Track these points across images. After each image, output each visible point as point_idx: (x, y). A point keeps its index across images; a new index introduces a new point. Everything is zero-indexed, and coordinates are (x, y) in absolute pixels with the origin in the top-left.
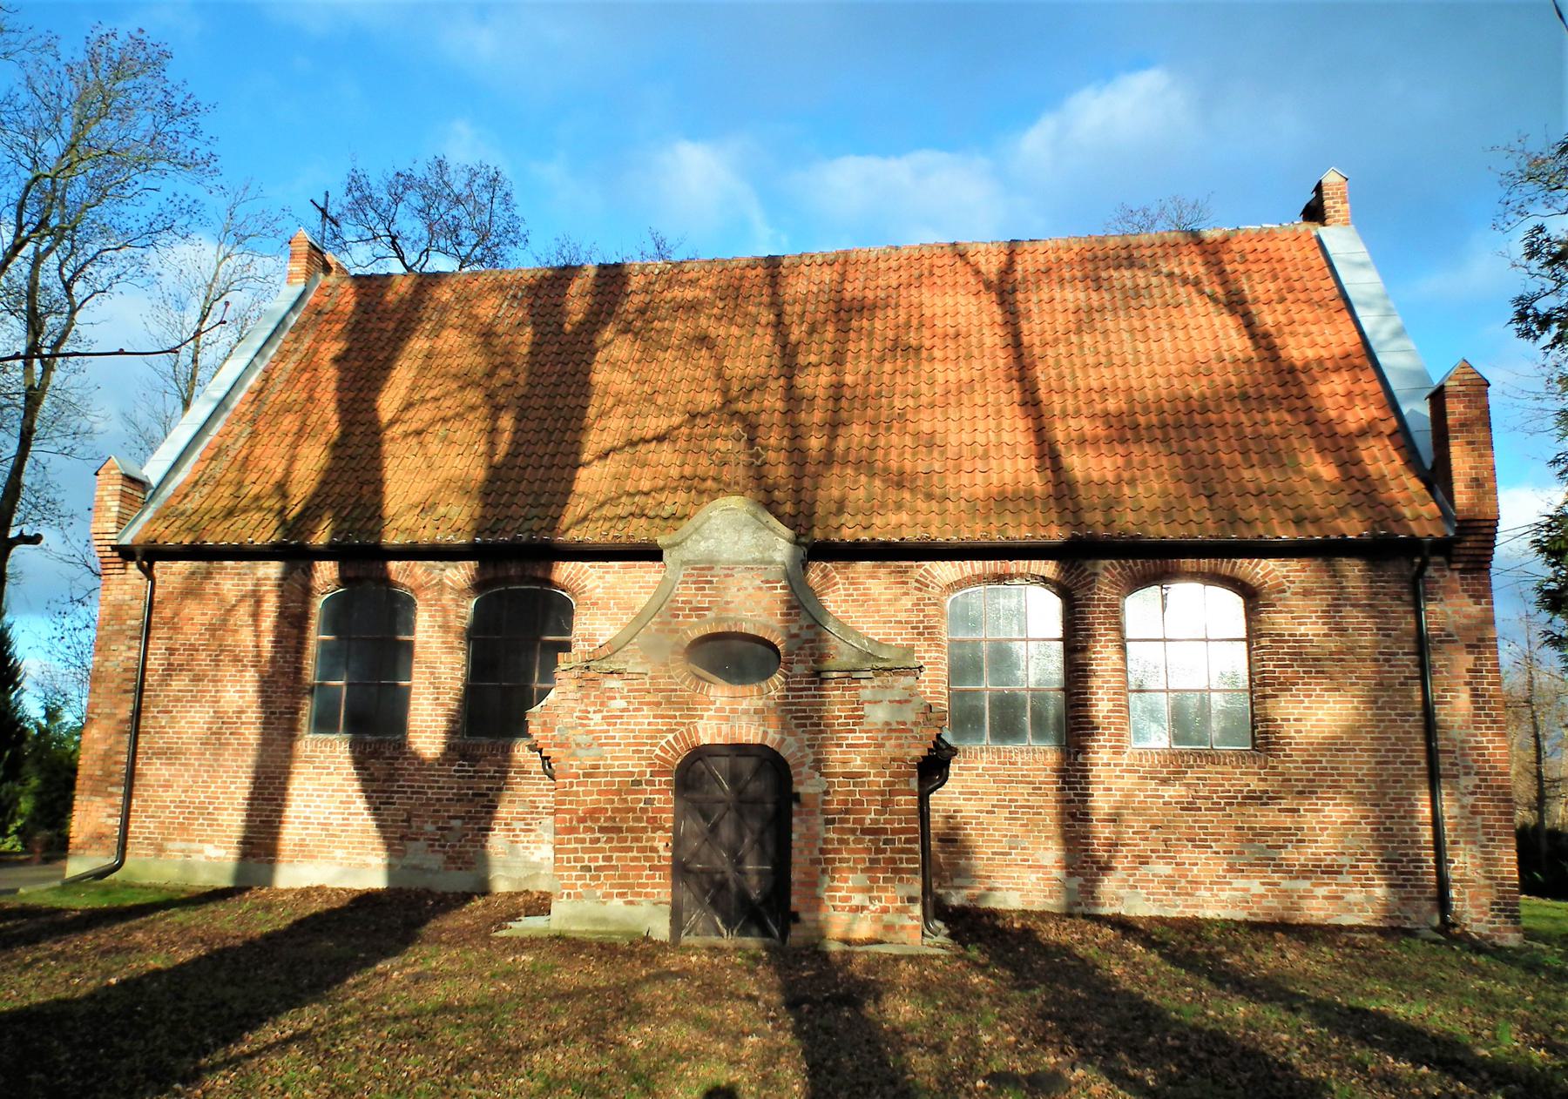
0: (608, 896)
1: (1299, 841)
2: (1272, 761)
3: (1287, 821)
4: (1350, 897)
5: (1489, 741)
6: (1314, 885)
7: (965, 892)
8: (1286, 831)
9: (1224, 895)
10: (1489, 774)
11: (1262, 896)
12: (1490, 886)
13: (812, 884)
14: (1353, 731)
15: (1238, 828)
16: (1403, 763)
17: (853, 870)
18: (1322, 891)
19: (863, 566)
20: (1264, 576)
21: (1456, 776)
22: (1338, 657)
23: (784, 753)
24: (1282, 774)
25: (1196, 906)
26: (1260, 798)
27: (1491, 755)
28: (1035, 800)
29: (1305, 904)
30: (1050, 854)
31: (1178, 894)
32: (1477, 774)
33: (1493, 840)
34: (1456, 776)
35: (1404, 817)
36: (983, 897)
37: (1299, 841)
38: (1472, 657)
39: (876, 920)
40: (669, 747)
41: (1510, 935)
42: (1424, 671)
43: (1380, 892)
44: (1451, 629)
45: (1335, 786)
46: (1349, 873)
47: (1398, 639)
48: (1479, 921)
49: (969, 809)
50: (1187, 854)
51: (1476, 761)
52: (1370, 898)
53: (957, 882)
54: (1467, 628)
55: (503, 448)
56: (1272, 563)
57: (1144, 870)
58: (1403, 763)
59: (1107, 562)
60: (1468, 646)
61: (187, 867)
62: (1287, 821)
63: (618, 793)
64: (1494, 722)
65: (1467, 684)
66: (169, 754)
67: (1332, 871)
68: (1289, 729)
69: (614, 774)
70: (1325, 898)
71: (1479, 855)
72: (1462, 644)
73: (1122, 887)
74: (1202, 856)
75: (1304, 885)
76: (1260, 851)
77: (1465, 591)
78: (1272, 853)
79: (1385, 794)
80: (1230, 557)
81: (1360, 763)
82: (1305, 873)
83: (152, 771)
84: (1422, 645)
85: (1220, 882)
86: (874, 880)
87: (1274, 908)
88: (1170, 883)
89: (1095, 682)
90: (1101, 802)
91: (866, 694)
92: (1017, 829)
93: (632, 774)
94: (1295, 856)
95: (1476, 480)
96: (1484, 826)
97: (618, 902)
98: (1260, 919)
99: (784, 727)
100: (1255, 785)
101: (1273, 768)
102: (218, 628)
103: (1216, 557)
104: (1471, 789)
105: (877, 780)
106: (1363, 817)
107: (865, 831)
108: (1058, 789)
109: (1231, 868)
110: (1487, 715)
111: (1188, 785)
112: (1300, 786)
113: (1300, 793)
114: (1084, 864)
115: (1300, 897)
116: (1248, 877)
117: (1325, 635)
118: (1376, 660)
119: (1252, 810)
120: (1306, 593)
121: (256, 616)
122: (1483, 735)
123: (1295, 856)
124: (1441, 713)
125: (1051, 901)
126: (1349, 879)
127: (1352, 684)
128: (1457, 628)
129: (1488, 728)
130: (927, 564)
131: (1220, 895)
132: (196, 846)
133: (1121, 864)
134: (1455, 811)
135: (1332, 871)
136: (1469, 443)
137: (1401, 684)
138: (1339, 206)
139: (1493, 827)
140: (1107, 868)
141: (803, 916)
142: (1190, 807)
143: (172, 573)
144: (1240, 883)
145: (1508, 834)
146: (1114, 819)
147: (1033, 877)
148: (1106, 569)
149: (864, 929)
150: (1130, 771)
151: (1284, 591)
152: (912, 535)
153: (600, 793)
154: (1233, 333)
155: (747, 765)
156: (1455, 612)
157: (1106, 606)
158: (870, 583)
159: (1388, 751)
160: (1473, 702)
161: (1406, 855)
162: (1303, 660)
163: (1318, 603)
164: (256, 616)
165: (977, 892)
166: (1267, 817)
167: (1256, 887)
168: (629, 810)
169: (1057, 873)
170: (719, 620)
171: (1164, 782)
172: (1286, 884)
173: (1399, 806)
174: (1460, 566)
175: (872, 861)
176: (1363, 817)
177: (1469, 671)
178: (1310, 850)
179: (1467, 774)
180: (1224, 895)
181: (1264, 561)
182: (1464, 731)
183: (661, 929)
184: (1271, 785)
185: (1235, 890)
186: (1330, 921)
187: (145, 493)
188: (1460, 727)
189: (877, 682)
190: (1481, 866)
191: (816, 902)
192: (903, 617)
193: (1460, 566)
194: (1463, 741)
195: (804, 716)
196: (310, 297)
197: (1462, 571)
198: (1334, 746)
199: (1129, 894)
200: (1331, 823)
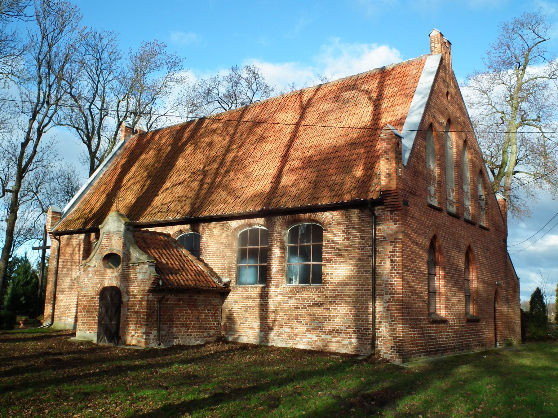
0: (86, 330)
1: (329, 320)
2: (323, 290)
3: (326, 313)
4: (344, 342)
5: (395, 281)
6: (333, 337)
7: (233, 336)
8: (324, 316)
9: (304, 340)
10: (394, 294)
11: (316, 341)
12: (391, 340)
13: (124, 328)
14: (350, 278)
15: (310, 315)
16: (365, 290)
17: (132, 324)
18: (334, 340)
19: (213, 224)
20: (325, 219)
21: (383, 295)
22: (346, 249)
23: (121, 289)
24: (325, 295)
25: (296, 344)
26: (318, 304)
27: (395, 286)
28: (253, 305)
29: (329, 344)
30: (256, 324)
31: (291, 339)
32: (390, 294)
33: (394, 321)
34: (383, 295)
35: (363, 312)
36: (237, 338)
37: (329, 320)
38: (392, 246)
39: (136, 339)
40: (98, 288)
41: (397, 360)
42: (375, 252)
43: (354, 341)
44: (385, 235)
45: (342, 299)
46: (344, 333)
47: (367, 241)
48: (386, 353)
49: (236, 307)
50: (294, 325)
51: (390, 289)
52: (350, 343)
53: (231, 333)
54: (391, 235)
55: (144, 191)
56: (328, 213)
57: (282, 330)
58: (365, 290)
59: (278, 217)
60: (391, 242)
61: (65, 324)
62: (326, 313)
63: (89, 301)
64: (397, 273)
65: (389, 258)
66: (63, 292)
67: (338, 332)
68: (328, 278)
69: (88, 296)
70: (336, 342)
71: (388, 327)
72: (389, 241)
73: (275, 336)
74: (298, 325)
75: (329, 337)
76: (317, 324)
77: (391, 219)
78: (320, 325)
79: (358, 302)
80: (314, 212)
81: (351, 291)
82: (330, 333)
83: (60, 296)
84: (375, 243)
85: (304, 335)
86: (136, 327)
87: (320, 346)
88: (289, 335)
89: (273, 261)
90: (272, 305)
91: (138, 270)
92: (248, 315)
93: (92, 295)
94: (328, 326)
95: (388, 174)
96: (391, 316)
97: (88, 332)
98: (315, 349)
99: (121, 282)
100: (317, 299)
101: (323, 292)
102: (72, 254)
103: (310, 213)
104: (387, 300)
105: (139, 297)
106: (350, 311)
107: (136, 312)
108: (260, 301)
109: (307, 330)
110: (395, 270)
111: (296, 299)
112: (330, 299)
113: (330, 302)
114: (266, 328)
115: (328, 342)
116: (312, 334)
117: (343, 240)
118: (359, 249)
119: (315, 308)
120: (338, 224)
121: (79, 250)
122: (393, 278)
123: (328, 326)
124: (379, 270)
125: (255, 340)
126: (344, 335)
127: (350, 259)
128: (388, 235)
129: (395, 276)
130: (229, 222)
131: (305, 341)
132: (66, 318)
133: (276, 328)
134: (381, 309)
135: (338, 332)
136: (387, 159)
137: (367, 259)
138: (436, 46)
139: (394, 316)
140: (272, 329)
141: (122, 337)
142: (297, 307)
143: (64, 238)
144: (309, 336)
145: (399, 319)
146: (275, 311)
147: (251, 332)
148: (278, 220)
149: (134, 342)
150: (280, 294)
151: (331, 224)
152: (227, 212)
153: (87, 301)
154: (369, 113)
155: (114, 293)
156: (388, 228)
157: (277, 233)
158: (214, 230)
159: (360, 285)
160: (391, 265)
161: (363, 326)
162: (335, 250)
163: (342, 228)
164: (79, 250)
165: (235, 336)
166: (319, 311)
167: (314, 337)
168: (91, 306)
169: (258, 331)
170: (110, 249)
171: (290, 298)
172: (323, 336)
173: (362, 307)
174: (389, 209)
175: (137, 321)
176: (350, 311)
177: (390, 252)
178: (334, 324)
179: (386, 294)
180: (304, 340)
181: (325, 213)
182: (386, 277)
183: (95, 340)
184: (321, 299)
185: (308, 338)
186: (337, 351)
187: (61, 216)
188: (385, 275)
189: (140, 267)
190: (389, 331)
191: (125, 334)
192: (222, 241)
193: (389, 209)
194: (387, 281)
195: (125, 278)
196: (126, 144)
197: (391, 211)
198: (344, 284)
199: (278, 340)
200: (341, 314)
